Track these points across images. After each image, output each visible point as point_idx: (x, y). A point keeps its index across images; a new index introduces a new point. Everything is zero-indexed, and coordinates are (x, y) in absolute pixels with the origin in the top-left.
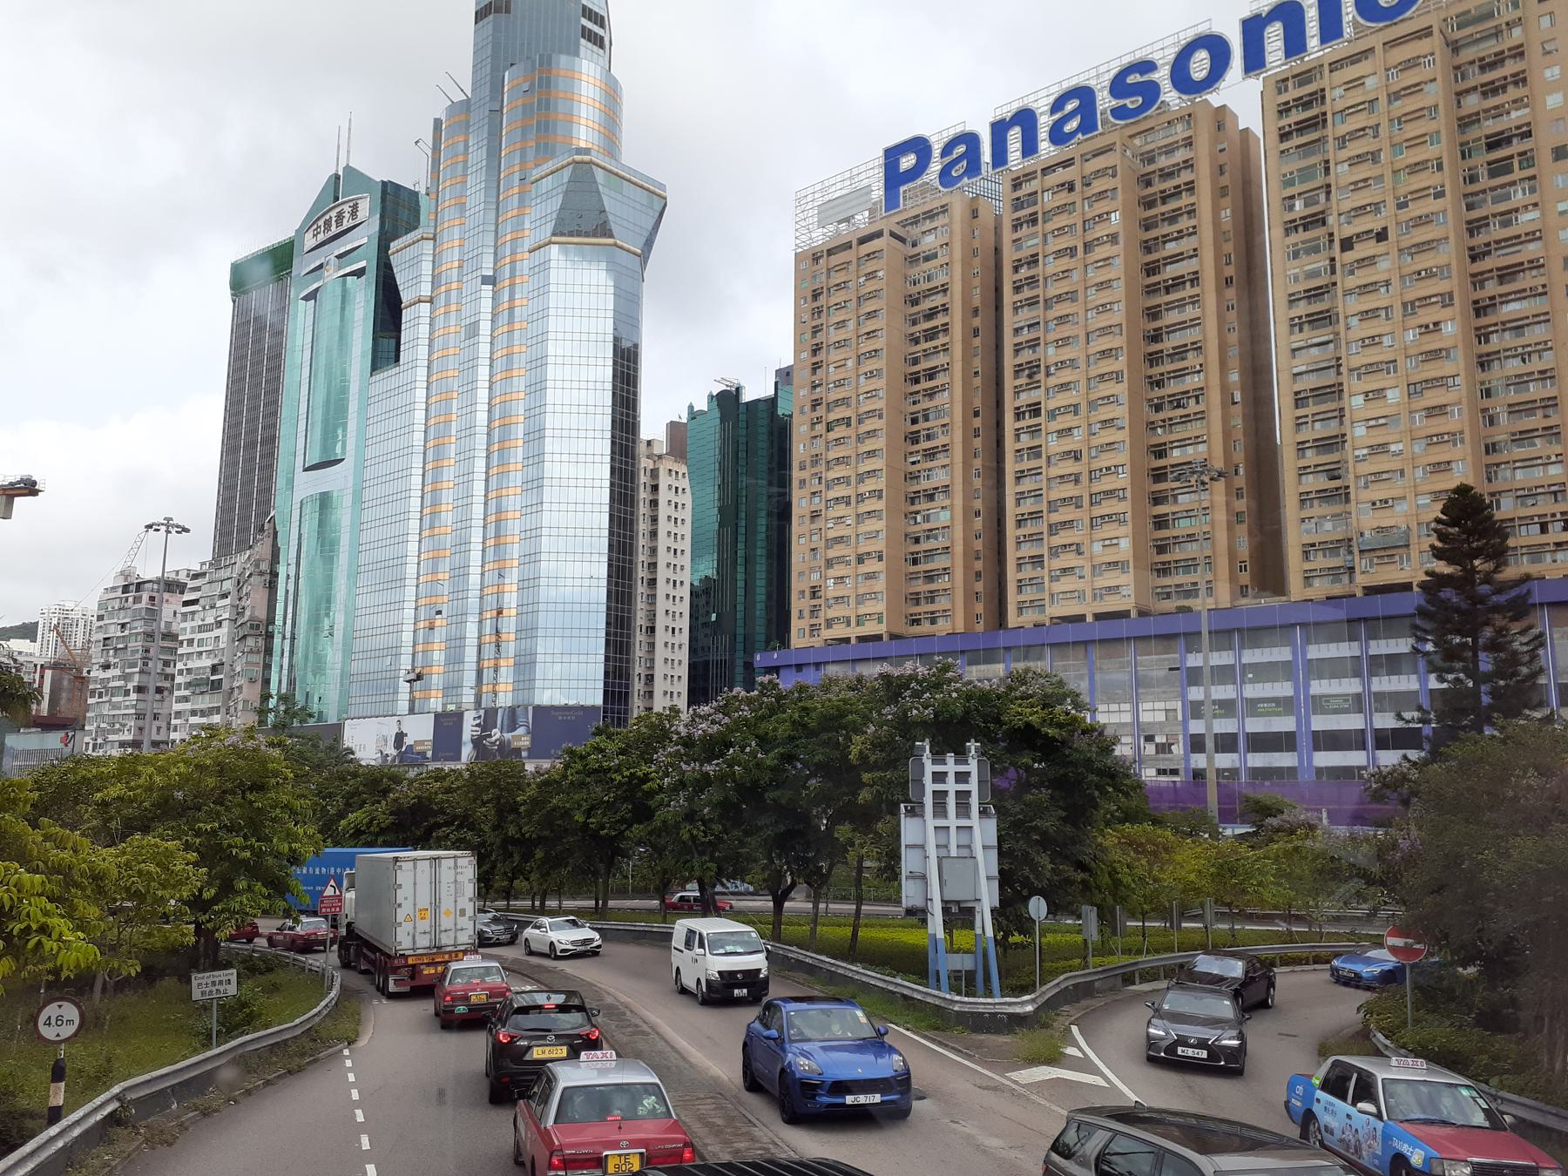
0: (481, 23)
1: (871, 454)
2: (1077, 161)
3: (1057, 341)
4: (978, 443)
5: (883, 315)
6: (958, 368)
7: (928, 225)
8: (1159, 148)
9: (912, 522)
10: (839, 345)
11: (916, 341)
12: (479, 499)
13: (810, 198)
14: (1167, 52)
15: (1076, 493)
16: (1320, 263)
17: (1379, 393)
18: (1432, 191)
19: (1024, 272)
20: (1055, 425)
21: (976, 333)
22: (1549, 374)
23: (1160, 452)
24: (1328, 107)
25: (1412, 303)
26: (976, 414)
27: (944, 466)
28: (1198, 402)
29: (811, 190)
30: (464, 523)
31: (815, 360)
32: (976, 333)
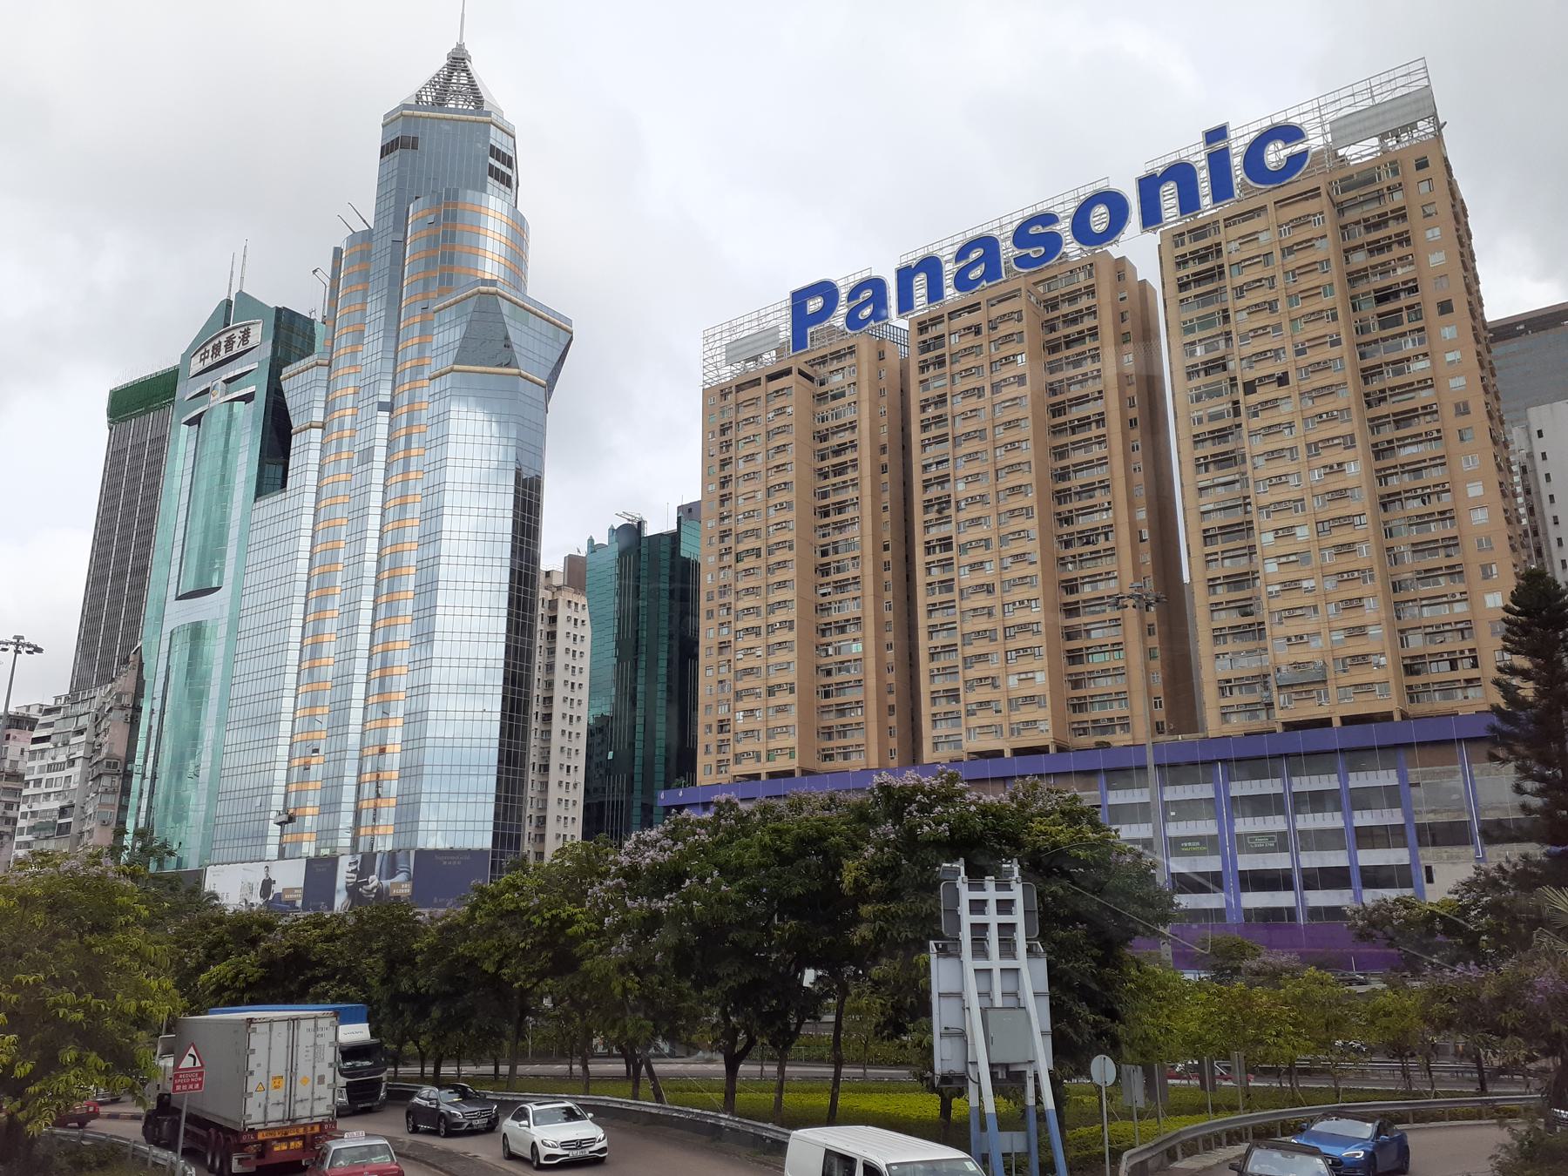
0: (387, 158)
1: (782, 585)
4: (888, 576)
6: (867, 502)
7: (835, 365)
9: (823, 654)
10: (749, 477)
13: (718, 337)
14: (1067, 206)
19: (931, 412)
21: (884, 469)
22: (1448, 515)
23: (1071, 587)
24: (1224, 260)
25: (1316, 444)
26: (886, 548)
27: (855, 599)
28: (1107, 539)
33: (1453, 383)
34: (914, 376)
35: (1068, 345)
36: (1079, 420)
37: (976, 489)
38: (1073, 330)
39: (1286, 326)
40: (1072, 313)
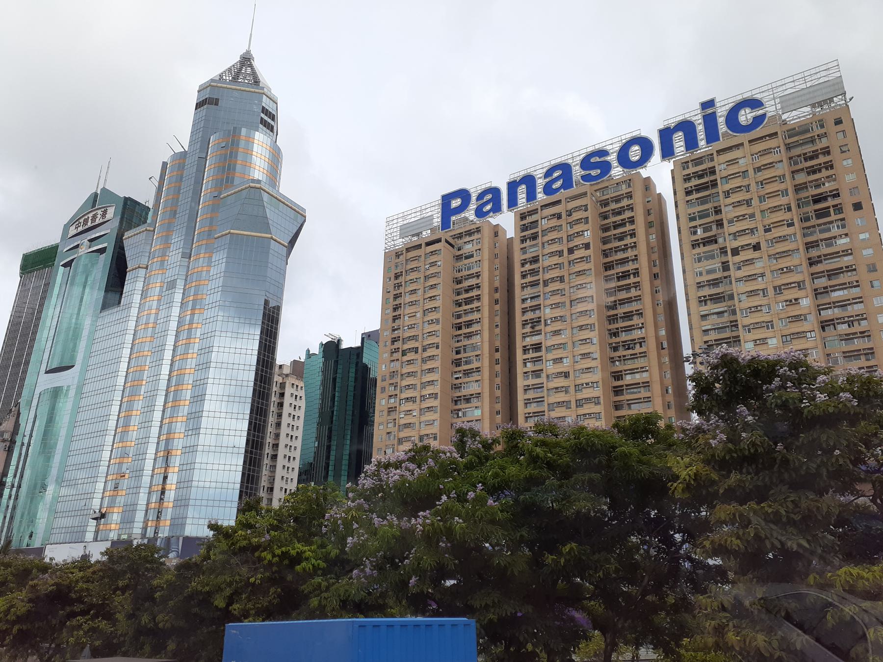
0: (199, 110)
1: (431, 370)
2: (563, 202)
3: (552, 305)
4: (498, 368)
5: (440, 287)
6: (486, 321)
7: (468, 239)
8: (611, 198)
9: (456, 416)
10: (412, 304)
11: (460, 305)
12: (156, 423)
13: (395, 221)
14: (614, 146)
15: (566, 399)
16: (716, 264)
17: (763, 341)
18: (785, 222)
19: (528, 267)
20: (551, 356)
21: (497, 302)
22: (866, 334)
23: (618, 376)
24: (718, 176)
25: (780, 287)
26: (497, 350)
27: (477, 381)
28: (641, 346)
29: (396, 217)
30: (143, 441)
31: (395, 314)
32: (497, 302)
33: (865, 252)
34: (517, 246)
35: (615, 227)
36: (622, 273)
37: (558, 313)
38: (619, 218)
39: (758, 215)
40: (618, 208)
